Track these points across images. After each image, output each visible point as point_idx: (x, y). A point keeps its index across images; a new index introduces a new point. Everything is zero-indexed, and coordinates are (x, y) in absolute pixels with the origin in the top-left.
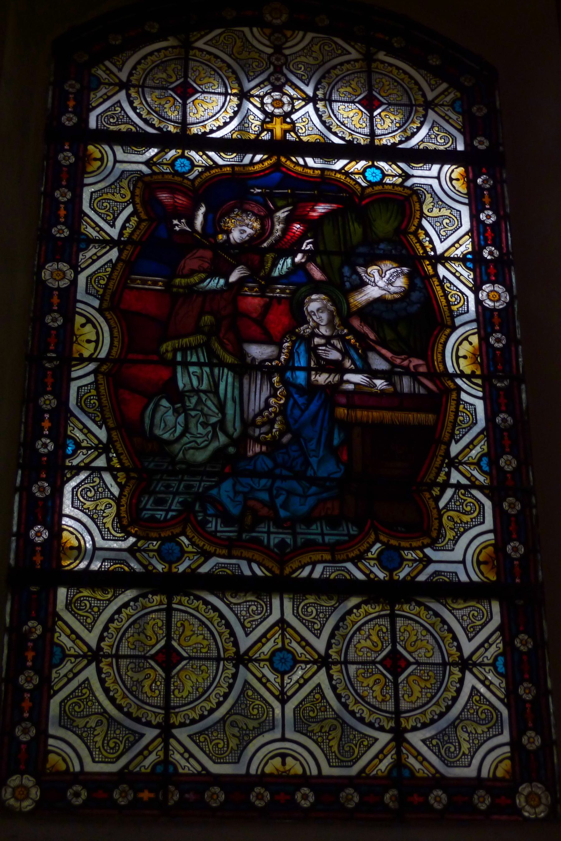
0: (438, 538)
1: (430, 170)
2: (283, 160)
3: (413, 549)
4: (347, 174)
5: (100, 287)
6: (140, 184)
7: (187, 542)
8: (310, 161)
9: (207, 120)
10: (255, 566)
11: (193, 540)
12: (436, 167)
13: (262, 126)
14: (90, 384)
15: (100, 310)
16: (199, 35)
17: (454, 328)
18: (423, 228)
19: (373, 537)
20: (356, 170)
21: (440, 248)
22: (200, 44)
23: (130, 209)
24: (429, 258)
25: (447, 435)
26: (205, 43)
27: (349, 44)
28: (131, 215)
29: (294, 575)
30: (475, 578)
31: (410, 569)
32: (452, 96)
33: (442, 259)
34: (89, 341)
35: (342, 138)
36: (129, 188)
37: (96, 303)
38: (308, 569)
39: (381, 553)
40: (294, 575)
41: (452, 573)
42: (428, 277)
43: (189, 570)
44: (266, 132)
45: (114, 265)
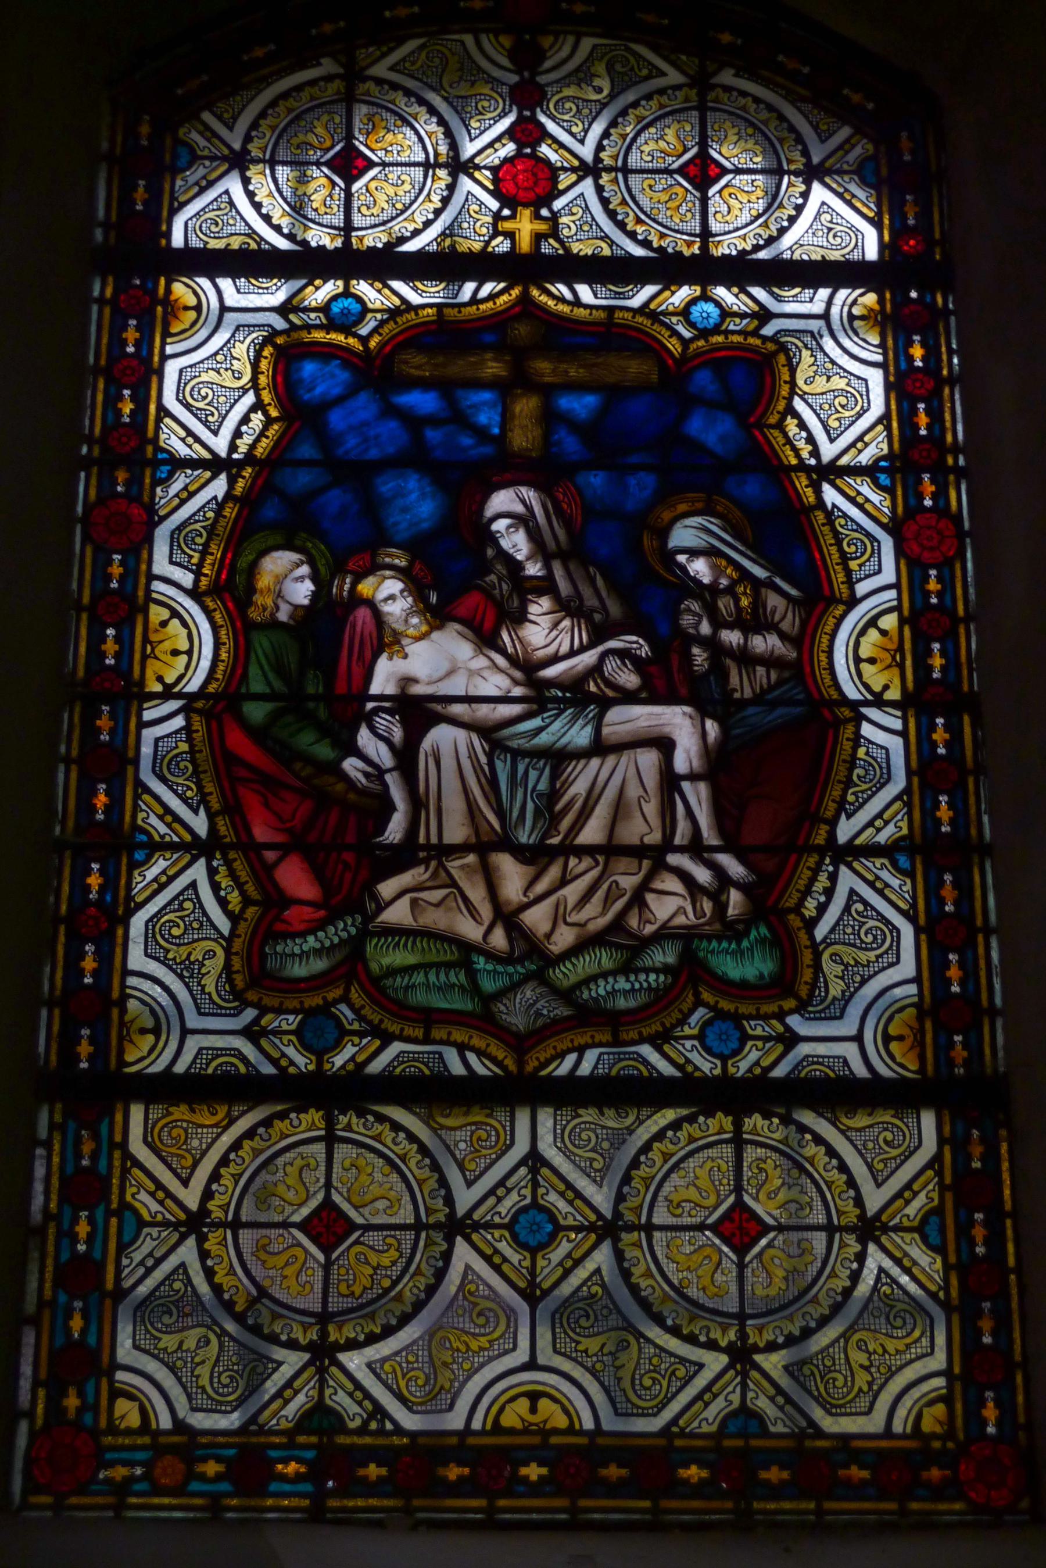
0: (263, 345)
1: (811, 300)
2: (535, 293)
3: (766, 1018)
4: (655, 316)
5: (194, 550)
6: (804, 991)
7: (350, 1015)
8: (585, 292)
9: (393, 219)
10: (472, 1058)
11: (363, 1012)
12: (823, 293)
13: (495, 225)
14: (177, 732)
15: (194, 593)
16: (378, 53)
17: (853, 602)
18: (796, 415)
19: (690, 998)
20: (671, 308)
21: (828, 451)
22: (380, 70)
23: (821, 931)
24: (225, 849)
25: (832, 806)
26: (392, 69)
27: (666, 59)
28: (253, 409)
29: (544, 1073)
30: (204, 282)
31: (760, 1053)
32: (858, 151)
33: (832, 472)
34: (175, 653)
35: (646, 244)
36: (824, 977)
37: (187, 579)
38: (571, 1059)
39: (706, 1025)
40: (544, 1073)
41: (838, 1057)
42: (225, 810)
43: (673, 288)
44: (500, 239)
45: (843, 808)
